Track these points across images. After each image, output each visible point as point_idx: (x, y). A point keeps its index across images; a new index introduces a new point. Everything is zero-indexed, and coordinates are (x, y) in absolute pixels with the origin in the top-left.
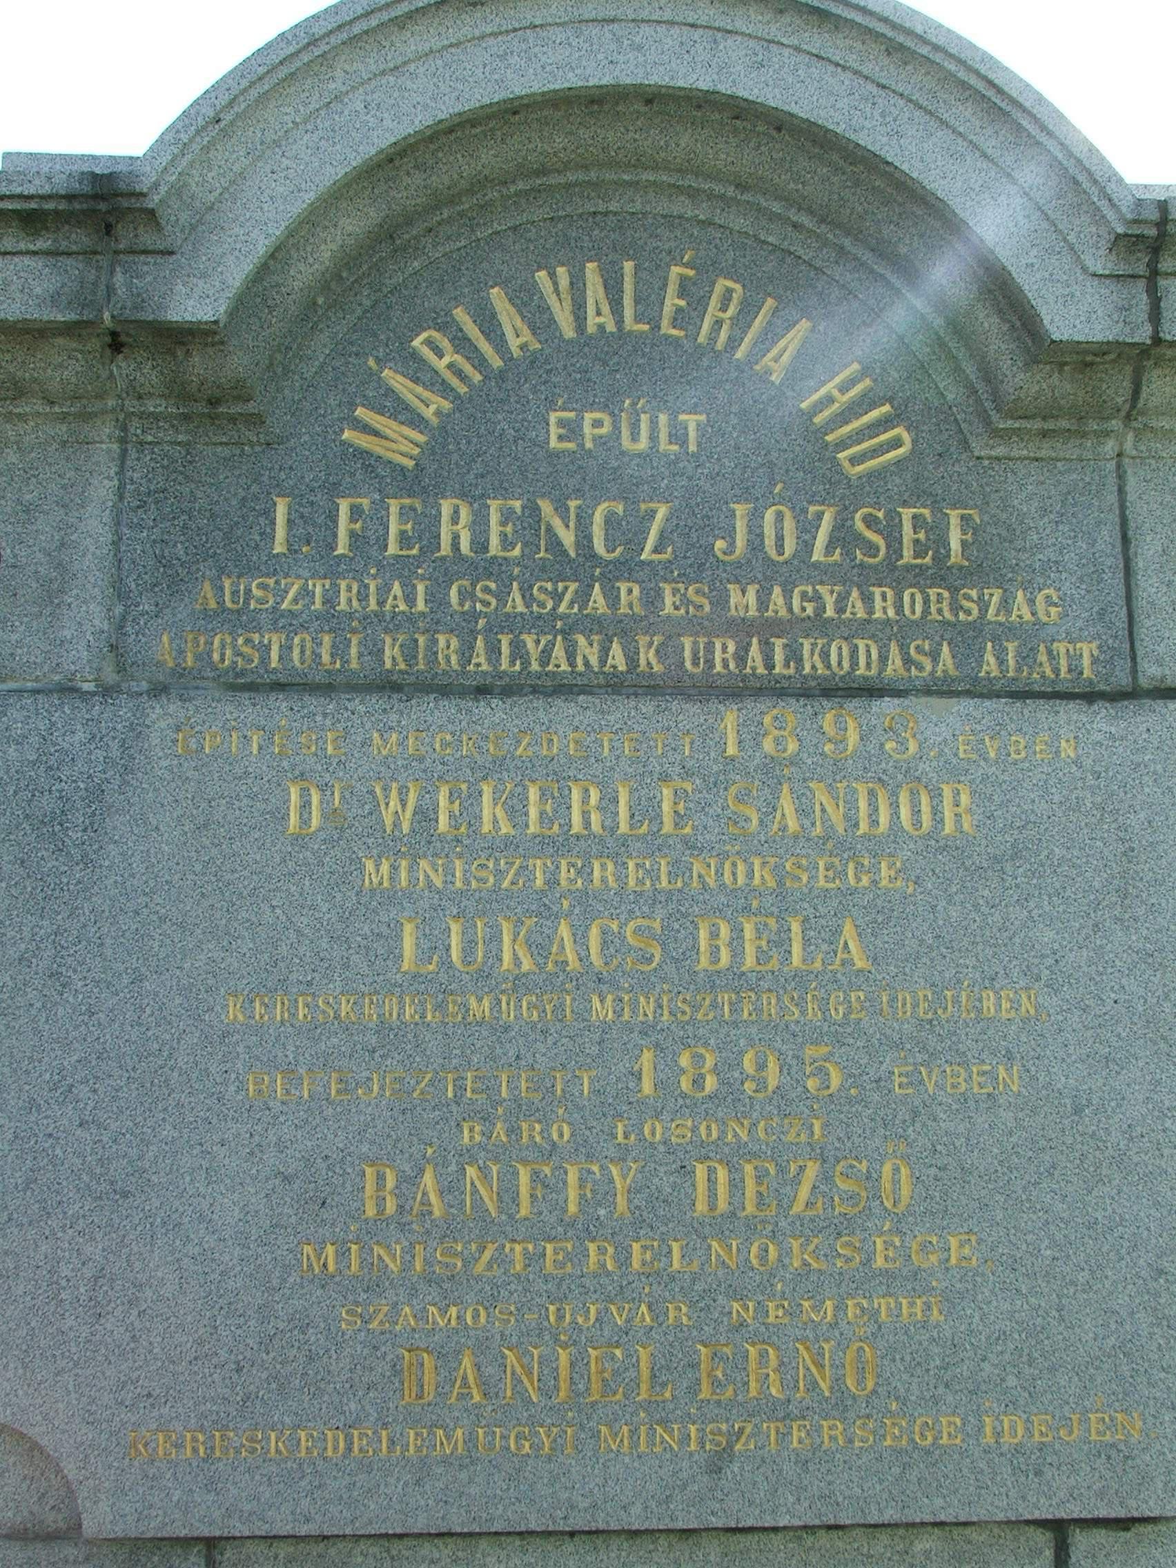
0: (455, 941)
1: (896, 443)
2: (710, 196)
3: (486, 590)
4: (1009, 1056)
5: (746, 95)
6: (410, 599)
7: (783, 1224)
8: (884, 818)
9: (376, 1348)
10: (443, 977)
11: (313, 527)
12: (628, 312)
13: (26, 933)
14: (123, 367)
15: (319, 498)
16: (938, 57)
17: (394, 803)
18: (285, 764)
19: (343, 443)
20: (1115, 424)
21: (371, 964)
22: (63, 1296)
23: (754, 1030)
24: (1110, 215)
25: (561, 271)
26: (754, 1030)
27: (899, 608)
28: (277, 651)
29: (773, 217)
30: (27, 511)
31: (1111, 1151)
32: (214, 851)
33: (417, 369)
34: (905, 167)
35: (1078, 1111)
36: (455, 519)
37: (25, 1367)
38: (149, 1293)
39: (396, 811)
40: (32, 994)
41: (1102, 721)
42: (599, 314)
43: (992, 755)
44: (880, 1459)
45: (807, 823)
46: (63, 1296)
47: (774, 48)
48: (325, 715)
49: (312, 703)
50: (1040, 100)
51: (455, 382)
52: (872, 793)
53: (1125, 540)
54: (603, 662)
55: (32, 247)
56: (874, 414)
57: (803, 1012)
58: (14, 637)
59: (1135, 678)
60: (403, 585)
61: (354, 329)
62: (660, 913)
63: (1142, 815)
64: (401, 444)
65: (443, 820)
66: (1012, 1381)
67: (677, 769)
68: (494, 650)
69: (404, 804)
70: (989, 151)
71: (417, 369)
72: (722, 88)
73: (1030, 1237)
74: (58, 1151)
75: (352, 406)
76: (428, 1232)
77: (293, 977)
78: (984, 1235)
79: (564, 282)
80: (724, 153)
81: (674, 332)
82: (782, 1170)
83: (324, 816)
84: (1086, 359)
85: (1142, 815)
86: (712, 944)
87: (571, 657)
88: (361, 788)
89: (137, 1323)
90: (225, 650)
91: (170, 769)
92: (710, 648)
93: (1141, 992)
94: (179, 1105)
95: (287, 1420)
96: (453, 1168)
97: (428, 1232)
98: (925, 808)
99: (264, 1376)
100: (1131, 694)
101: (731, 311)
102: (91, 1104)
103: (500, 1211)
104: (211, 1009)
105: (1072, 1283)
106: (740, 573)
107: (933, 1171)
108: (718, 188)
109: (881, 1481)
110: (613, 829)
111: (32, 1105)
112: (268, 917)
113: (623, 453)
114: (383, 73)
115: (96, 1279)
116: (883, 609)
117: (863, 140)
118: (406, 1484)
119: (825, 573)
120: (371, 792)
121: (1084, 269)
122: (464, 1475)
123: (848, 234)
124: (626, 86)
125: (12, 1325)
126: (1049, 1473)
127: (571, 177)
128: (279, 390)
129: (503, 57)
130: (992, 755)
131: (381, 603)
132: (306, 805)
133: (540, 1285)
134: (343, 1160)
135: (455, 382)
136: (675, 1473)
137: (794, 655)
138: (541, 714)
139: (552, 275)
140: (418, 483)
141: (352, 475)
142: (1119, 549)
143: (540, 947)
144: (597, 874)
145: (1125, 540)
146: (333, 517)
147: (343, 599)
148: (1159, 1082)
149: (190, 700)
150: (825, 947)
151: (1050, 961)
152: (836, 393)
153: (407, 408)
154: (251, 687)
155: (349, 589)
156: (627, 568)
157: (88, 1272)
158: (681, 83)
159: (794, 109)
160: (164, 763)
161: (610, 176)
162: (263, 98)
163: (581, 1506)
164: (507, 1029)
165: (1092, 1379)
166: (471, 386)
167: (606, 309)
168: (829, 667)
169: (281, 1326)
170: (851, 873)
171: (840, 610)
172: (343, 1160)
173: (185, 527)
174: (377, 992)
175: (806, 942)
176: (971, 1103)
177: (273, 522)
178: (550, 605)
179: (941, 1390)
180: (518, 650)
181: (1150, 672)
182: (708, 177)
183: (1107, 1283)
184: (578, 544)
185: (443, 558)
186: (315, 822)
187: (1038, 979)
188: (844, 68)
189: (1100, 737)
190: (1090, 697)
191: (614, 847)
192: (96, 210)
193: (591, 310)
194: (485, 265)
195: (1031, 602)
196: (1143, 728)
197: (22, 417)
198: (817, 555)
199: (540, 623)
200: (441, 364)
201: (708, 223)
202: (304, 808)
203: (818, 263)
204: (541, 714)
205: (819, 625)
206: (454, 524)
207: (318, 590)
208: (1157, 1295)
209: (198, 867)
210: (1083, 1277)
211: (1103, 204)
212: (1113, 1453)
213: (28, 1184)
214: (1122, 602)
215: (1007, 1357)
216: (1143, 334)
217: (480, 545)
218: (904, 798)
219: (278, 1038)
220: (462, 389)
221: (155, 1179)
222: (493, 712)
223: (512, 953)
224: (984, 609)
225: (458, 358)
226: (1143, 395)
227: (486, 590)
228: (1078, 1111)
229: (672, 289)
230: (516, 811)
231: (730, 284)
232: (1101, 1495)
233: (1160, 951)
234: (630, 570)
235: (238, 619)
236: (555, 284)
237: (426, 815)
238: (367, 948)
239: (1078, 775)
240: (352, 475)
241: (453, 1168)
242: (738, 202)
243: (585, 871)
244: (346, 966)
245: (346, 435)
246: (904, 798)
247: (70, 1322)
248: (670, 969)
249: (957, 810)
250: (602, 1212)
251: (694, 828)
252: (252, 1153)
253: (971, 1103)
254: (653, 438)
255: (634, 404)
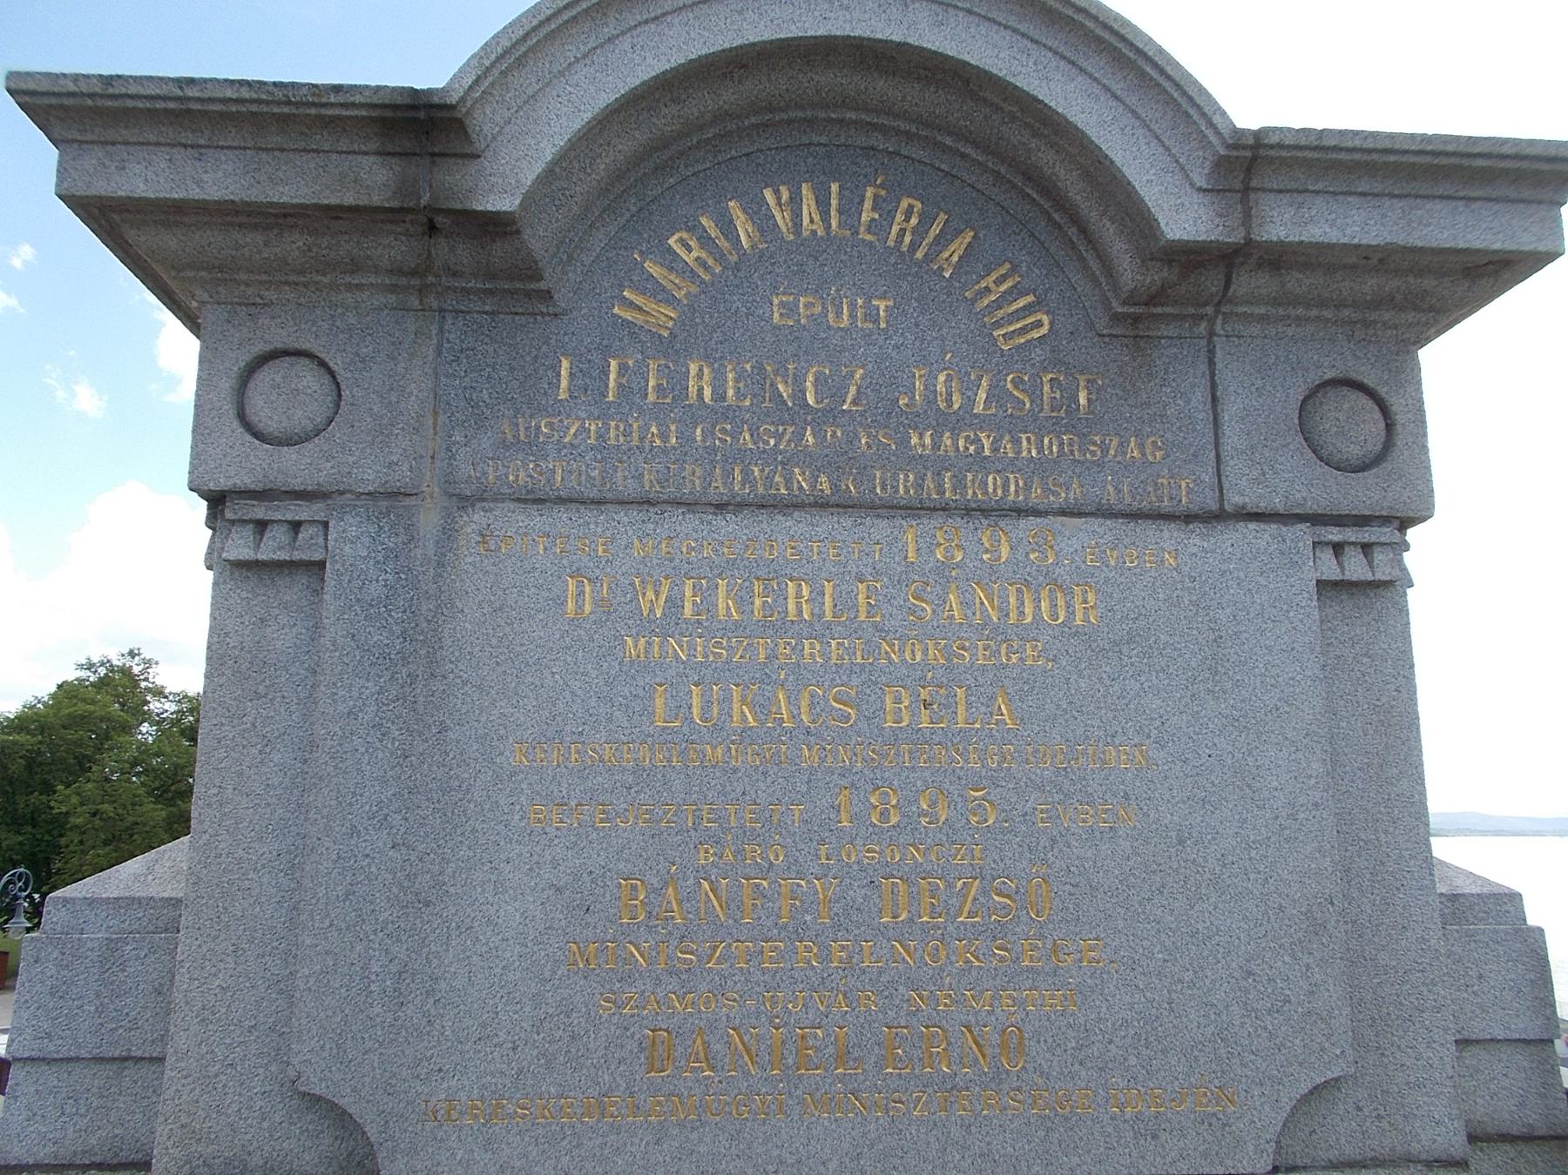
0: (696, 701)
1: (1039, 324)
2: (898, 132)
3: (724, 431)
4: (1126, 797)
5: (929, 46)
6: (664, 437)
7: (950, 928)
8: (1028, 610)
9: (627, 1029)
10: (685, 729)
11: (590, 380)
12: (834, 223)
13: (355, 694)
14: (442, 250)
15: (596, 357)
16: (1079, 17)
17: (650, 595)
18: (565, 561)
19: (614, 315)
20: (1209, 310)
21: (630, 718)
22: (373, 988)
23: (927, 774)
24: (1213, 138)
25: (783, 189)
26: (927, 774)
27: (1040, 450)
28: (560, 476)
29: (946, 149)
30: (363, 361)
31: (1208, 875)
32: (508, 629)
33: (671, 260)
34: (1052, 104)
35: (1181, 842)
36: (700, 375)
37: (338, 1047)
38: (443, 984)
39: (653, 602)
40: (357, 741)
41: (1196, 540)
42: (812, 221)
43: (1113, 563)
44: (1028, 1124)
45: (969, 613)
46: (373, 988)
47: (951, 10)
48: (597, 524)
49: (588, 515)
50: (1161, 51)
51: (701, 272)
52: (1019, 591)
53: (1214, 399)
54: (813, 487)
55: (364, 148)
56: (1021, 303)
57: (967, 761)
58: (351, 459)
59: (1222, 504)
60: (659, 425)
61: (623, 228)
62: (855, 681)
63: (1228, 611)
64: (663, 316)
65: (688, 606)
66: (1133, 1061)
67: (870, 570)
68: (728, 474)
69: (657, 594)
70: (1119, 92)
71: (671, 260)
72: (910, 40)
73: (1145, 943)
74: (373, 869)
75: (621, 287)
76: (670, 933)
77: (568, 728)
78: (1108, 941)
79: (785, 196)
80: (910, 95)
81: (868, 237)
82: (950, 886)
83: (595, 603)
84: (1190, 258)
85: (1228, 611)
86: (897, 709)
87: (788, 482)
88: (625, 581)
89: (433, 1012)
90: (520, 473)
91: (473, 564)
92: (895, 478)
93: (1230, 748)
94: (474, 830)
95: (553, 1090)
96: (691, 881)
97: (670, 933)
98: (1061, 603)
99: (535, 1053)
100: (1218, 516)
101: (914, 221)
102: (403, 830)
103: (728, 916)
104: (501, 754)
105: (1180, 981)
106: (916, 421)
107: (1068, 887)
108: (904, 126)
109: (1029, 1142)
110: (821, 616)
111: (354, 831)
112: (549, 681)
113: (829, 327)
114: (646, 22)
115: (401, 973)
116: (1028, 450)
117: (1020, 82)
118: (648, 1143)
119: (982, 423)
120: (632, 584)
121: (1192, 185)
122: (694, 1136)
123: (1003, 162)
124: (836, 37)
125: (330, 1013)
126: (1163, 1136)
127: (792, 114)
128: (565, 273)
129: (741, 12)
130: (1113, 563)
131: (641, 439)
132: (581, 593)
133: (758, 976)
134: (603, 876)
135: (701, 272)
136: (864, 1134)
137: (959, 484)
138: (764, 525)
139: (777, 192)
140: (672, 348)
141: (621, 340)
142: (1209, 406)
143: (763, 708)
144: (807, 651)
145: (1214, 399)
146: (605, 372)
147: (612, 434)
148: (1245, 821)
149: (491, 510)
150: (983, 709)
151: (1158, 723)
152: (992, 285)
153: (664, 289)
154: (539, 501)
155: (617, 427)
156: (830, 415)
157: (394, 968)
158: (879, 36)
159: (966, 58)
160: (469, 560)
161: (822, 115)
162: (551, 35)
163: (790, 1161)
164: (735, 771)
165: (1196, 1059)
166: (713, 275)
167: (817, 218)
168: (986, 493)
169: (550, 1011)
170: (1003, 651)
171: (995, 450)
172: (603, 876)
173: (489, 376)
174: (633, 742)
175: (969, 705)
176: (1097, 834)
177: (559, 375)
178: (772, 442)
179: (1077, 1066)
180: (747, 478)
181: (1234, 499)
182: (897, 116)
183: (1207, 982)
184: (793, 396)
185: (690, 406)
186: (588, 608)
187: (1149, 737)
188: (1006, 27)
189: (1195, 550)
190: (1188, 518)
191: (819, 630)
192: (418, 126)
193: (806, 221)
194: (725, 183)
195: (1141, 447)
196: (1228, 544)
197: (359, 287)
198: (979, 408)
199: (768, 457)
200: (689, 258)
201: (897, 153)
202: (580, 599)
203: (980, 187)
204: (764, 525)
205: (980, 463)
206: (699, 381)
207: (593, 428)
208: (1247, 991)
209: (494, 641)
210: (1189, 975)
211: (1209, 133)
212: (1214, 1121)
213: (347, 894)
214: (1211, 447)
215: (1129, 1040)
216: (1237, 237)
217: (719, 396)
218: (1044, 594)
219: (554, 777)
220: (707, 278)
221: (452, 890)
222: (727, 525)
223: (743, 714)
224: (1105, 451)
225: (704, 255)
226: (1233, 287)
227: (724, 431)
228: (1181, 842)
229: (868, 204)
230: (743, 602)
231: (911, 201)
232: (1205, 1155)
233: (1245, 716)
234: (835, 417)
235: (532, 447)
236: (779, 199)
237: (674, 604)
238: (627, 706)
239: (1178, 579)
240: (621, 340)
241: (691, 881)
242: (920, 137)
243: (797, 649)
244: (610, 720)
245: (616, 310)
246: (1044, 594)
247: (378, 1010)
248: (863, 725)
249: (1085, 609)
250: (808, 918)
251: (883, 616)
252: (531, 869)
253: (1097, 834)
254: (852, 316)
255: (838, 290)
